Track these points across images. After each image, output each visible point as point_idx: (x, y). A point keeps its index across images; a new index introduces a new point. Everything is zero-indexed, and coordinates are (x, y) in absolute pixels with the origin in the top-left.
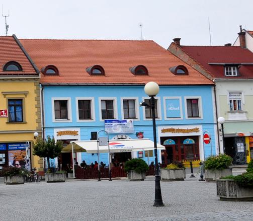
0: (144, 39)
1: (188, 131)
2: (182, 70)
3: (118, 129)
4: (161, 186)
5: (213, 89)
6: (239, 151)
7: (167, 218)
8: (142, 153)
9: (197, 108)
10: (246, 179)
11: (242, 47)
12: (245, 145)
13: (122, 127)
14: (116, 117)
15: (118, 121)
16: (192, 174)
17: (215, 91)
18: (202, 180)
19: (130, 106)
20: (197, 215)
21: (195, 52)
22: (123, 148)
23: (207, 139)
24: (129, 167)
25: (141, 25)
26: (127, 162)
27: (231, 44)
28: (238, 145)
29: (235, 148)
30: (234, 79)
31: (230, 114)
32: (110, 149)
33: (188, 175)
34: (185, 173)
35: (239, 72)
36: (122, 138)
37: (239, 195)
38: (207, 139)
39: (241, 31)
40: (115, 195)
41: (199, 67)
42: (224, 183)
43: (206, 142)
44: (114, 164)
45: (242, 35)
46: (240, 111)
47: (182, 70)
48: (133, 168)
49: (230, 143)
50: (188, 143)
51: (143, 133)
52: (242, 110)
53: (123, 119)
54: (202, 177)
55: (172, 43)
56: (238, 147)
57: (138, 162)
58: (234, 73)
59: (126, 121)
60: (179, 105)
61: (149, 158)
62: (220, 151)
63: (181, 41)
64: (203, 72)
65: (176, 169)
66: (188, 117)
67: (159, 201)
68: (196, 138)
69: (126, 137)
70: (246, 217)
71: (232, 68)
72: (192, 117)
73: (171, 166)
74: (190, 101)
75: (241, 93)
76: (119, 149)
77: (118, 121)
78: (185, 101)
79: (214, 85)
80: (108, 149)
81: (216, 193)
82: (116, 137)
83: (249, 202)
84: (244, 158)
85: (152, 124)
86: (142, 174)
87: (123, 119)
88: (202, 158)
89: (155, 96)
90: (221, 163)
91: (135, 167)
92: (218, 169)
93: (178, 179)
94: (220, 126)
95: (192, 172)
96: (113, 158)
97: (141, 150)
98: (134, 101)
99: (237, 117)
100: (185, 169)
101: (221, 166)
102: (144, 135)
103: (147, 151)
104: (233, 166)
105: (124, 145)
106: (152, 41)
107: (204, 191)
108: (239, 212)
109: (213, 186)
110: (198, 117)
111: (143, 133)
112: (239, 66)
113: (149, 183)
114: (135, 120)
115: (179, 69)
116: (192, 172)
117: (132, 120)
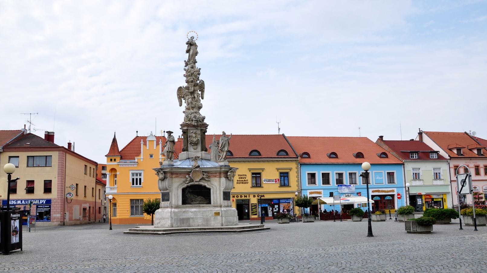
0: (362, 136)
1: (388, 191)
2: (384, 155)
3: (346, 190)
5: (403, 166)
8: (360, 205)
9: (393, 178)
10: (423, 220)
12: (422, 200)
13: (349, 189)
14: (345, 183)
15: (346, 186)
16: (390, 217)
17: (404, 167)
18: (396, 221)
19: (353, 177)
20: (393, 242)
21: (392, 144)
22: (349, 202)
24: (352, 213)
27: (414, 140)
29: (416, 202)
31: (413, 181)
33: (388, 218)
36: (348, 196)
37: (419, 230)
39: (420, 131)
40: (344, 230)
41: (394, 153)
43: (399, 198)
44: (344, 211)
45: (420, 134)
46: (419, 179)
47: (384, 155)
48: (355, 214)
49: (413, 198)
50: (388, 199)
51: (361, 192)
52: (420, 179)
53: (349, 184)
54: (396, 219)
56: (418, 201)
58: (416, 157)
63: (383, 138)
64: (397, 156)
66: (388, 183)
67: (370, 234)
68: (393, 196)
69: (351, 195)
70: (423, 243)
72: (390, 183)
73: (378, 213)
74: (389, 174)
75: (420, 169)
76: (346, 202)
77: (346, 186)
78: (386, 174)
79: (403, 164)
81: (405, 229)
84: (422, 208)
85: (366, 187)
86: (360, 217)
90: (408, 211)
91: (356, 213)
92: (406, 214)
93: (382, 221)
94: (407, 189)
95: (390, 216)
97: (360, 203)
98: (355, 173)
99: (417, 183)
100: (386, 214)
101: (408, 213)
102: (361, 194)
103: (363, 204)
105: (349, 200)
106: (366, 138)
110: (394, 183)
111: (361, 192)
112: (418, 153)
113: (365, 223)
116: (390, 216)
117: (354, 185)
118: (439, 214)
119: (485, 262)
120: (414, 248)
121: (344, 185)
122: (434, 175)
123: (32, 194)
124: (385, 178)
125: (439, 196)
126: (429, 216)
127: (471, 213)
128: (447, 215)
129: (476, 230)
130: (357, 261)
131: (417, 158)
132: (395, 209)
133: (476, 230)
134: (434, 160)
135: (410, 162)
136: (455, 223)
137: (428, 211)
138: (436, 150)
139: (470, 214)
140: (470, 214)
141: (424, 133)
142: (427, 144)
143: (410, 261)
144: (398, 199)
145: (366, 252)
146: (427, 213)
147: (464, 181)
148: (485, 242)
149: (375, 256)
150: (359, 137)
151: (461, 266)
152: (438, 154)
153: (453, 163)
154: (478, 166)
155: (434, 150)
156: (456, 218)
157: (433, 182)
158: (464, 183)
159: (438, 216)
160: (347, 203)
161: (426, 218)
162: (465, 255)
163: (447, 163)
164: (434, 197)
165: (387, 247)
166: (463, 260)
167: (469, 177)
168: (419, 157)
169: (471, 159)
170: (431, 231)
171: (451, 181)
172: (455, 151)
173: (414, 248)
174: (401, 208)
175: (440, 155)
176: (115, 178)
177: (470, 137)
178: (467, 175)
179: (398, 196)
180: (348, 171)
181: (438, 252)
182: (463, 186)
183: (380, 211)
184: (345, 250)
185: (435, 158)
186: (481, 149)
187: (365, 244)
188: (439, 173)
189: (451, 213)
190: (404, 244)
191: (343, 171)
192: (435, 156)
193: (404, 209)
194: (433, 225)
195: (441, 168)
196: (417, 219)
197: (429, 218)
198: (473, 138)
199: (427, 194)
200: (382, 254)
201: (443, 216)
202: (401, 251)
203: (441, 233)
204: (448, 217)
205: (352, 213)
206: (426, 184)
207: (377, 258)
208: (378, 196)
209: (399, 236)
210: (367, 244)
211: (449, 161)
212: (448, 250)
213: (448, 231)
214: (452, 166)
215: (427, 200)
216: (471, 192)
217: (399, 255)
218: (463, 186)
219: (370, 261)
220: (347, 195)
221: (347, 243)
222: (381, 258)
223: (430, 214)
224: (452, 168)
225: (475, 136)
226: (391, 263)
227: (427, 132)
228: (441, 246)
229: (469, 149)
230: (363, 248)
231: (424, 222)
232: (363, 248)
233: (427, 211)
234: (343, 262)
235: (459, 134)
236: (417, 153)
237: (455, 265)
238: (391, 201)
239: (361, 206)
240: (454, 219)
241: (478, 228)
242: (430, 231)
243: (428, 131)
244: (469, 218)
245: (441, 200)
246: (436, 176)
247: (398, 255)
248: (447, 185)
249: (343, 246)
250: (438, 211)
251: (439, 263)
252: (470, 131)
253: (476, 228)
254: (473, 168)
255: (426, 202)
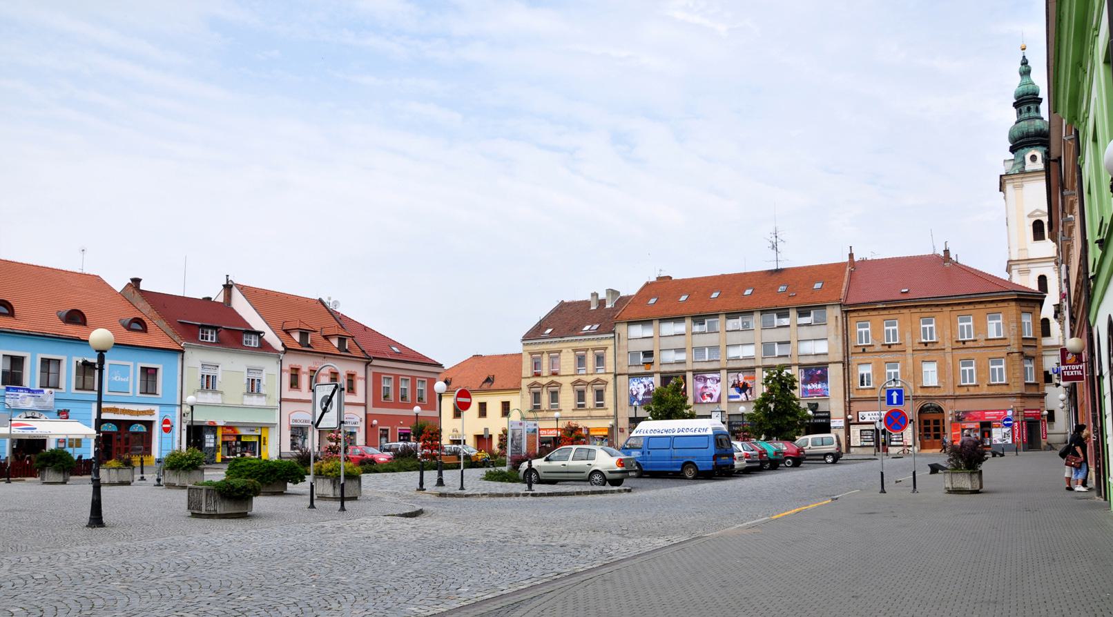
0: (87, 271)
1: (138, 413)
2: (138, 324)
3: (29, 402)
4: (102, 494)
5: (180, 356)
6: (207, 445)
7: (111, 548)
8: (64, 441)
9: (155, 381)
10: (233, 487)
11: (226, 305)
12: (216, 438)
13: (36, 401)
14: (27, 382)
15: (29, 390)
16: (141, 475)
17: (183, 359)
18: (159, 485)
19: (52, 368)
20: (159, 541)
21: (160, 302)
22: (35, 432)
23: (168, 426)
24: (43, 463)
25: (83, 250)
26: (40, 454)
27: (211, 299)
28: (207, 437)
29: (203, 441)
30: (211, 346)
31: (199, 393)
32: (12, 433)
33: (138, 476)
34: (133, 475)
35: (218, 338)
36: (33, 417)
37: (220, 510)
38: (168, 426)
39: (228, 282)
40: (18, 507)
41: (163, 324)
42: (199, 491)
43: (167, 430)
44: (16, 457)
45: (228, 287)
46: (214, 390)
47: (138, 324)
48: (50, 464)
49: (196, 433)
50: (136, 430)
51: (69, 411)
52: (217, 389)
53: (38, 388)
54: (159, 480)
55: (129, 283)
56: (207, 441)
57: (59, 456)
58: (212, 338)
59: (42, 391)
60: (129, 375)
61: (467, 471)
62: (181, 444)
63: (141, 283)
64: (169, 331)
65: (119, 468)
66: (141, 393)
67: (96, 518)
68: (149, 424)
69: (41, 416)
70: (234, 544)
71: (210, 331)
72: (147, 393)
73: (113, 463)
74: (145, 370)
75: (218, 366)
76: (26, 434)
77: (29, 390)
78: (139, 370)
79: (182, 352)
80: (9, 432)
81: (186, 507)
82: (23, 415)
83: (234, 520)
84: (213, 455)
85: (96, 399)
86: (64, 473)
87: (38, 388)
88: (156, 453)
89: (106, 351)
90: (190, 462)
91: (54, 463)
92: (184, 469)
93: (122, 483)
94: (186, 409)
95: (142, 473)
96: (15, 447)
97: (64, 437)
98: (59, 361)
99: (209, 398)
100: (134, 467)
101: (189, 466)
102: (70, 414)
103: (73, 439)
104: (207, 466)
105: (36, 429)
106: (98, 276)
107: (164, 502)
108: (222, 535)
109: (184, 494)
110: (155, 394)
111: (69, 411)
112: (219, 330)
113: (80, 489)
114: (57, 390)
115: (135, 322)
116: (142, 473)
117: (53, 390)
118: (262, 471)
119: (385, 589)
120: (216, 558)
121: (24, 389)
122: (248, 383)
123: (1049, 338)
124: (134, 381)
125: (254, 431)
126: (240, 476)
127: (331, 472)
128: (281, 476)
129: (343, 509)
130: (63, 605)
131: (214, 341)
132: (150, 454)
133: (343, 509)
134: (252, 351)
135: (198, 348)
136: (293, 492)
137: (239, 464)
138: (257, 328)
139: (329, 474)
140: (329, 474)
141: (237, 288)
142: (240, 314)
143: (214, 594)
144: (164, 433)
145: (86, 572)
146: (236, 468)
147: (329, 401)
148: (370, 537)
149: (116, 584)
150: (80, 274)
151: (339, 603)
152: (260, 338)
153: (290, 361)
154: (297, 370)
155: (252, 328)
156: (297, 483)
157: (243, 398)
158: (327, 405)
159: (260, 477)
160: (29, 435)
161: (239, 482)
162: (338, 573)
163: (277, 360)
164: (242, 432)
165: (145, 556)
166: (341, 587)
167: (341, 391)
168: (261, 344)
169: (325, 358)
170: (249, 513)
171: (281, 400)
172: (296, 336)
173: (216, 558)
174: (173, 455)
175: (264, 339)
176: (868, 375)
177: (328, 310)
178: (336, 387)
179: (165, 426)
180: (41, 353)
181: (278, 567)
182: (325, 411)
183: (120, 459)
184: (21, 568)
185: (253, 345)
186: (345, 339)
187: (81, 547)
188: (259, 380)
189: (288, 471)
190: (188, 546)
191: (62, 355)
192: (254, 342)
193: (181, 456)
194: (254, 498)
195: (220, 366)
196: (218, 483)
197: (246, 482)
198: (333, 314)
199: (229, 425)
200: (134, 577)
201: (272, 476)
202: (185, 566)
203: (269, 517)
204: (282, 480)
205: (43, 463)
206: (228, 402)
207: (121, 591)
208: (113, 423)
209: (172, 526)
210: (88, 547)
211: (282, 355)
212: (297, 559)
213: (284, 512)
214: (286, 367)
215: (227, 439)
216: (340, 424)
217: (182, 579)
218: (325, 411)
219: (101, 602)
220: (29, 414)
221: (29, 548)
222: (134, 589)
223: (243, 471)
224: (305, 375)
225: (337, 310)
226: (163, 603)
227: (244, 286)
228: (280, 550)
229: (323, 336)
230: (78, 562)
231: (234, 490)
232: (78, 562)
233: (236, 465)
234: (17, 609)
235: (307, 300)
236: (216, 330)
237: (326, 601)
238: (142, 437)
239: (67, 444)
240: (294, 483)
241: (347, 504)
242: (247, 513)
243: (244, 284)
244: (328, 482)
245: (255, 439)
246: (252, 386)
247: (179, 578)
248: (273, 409)
249: (14, 559)
250: (262, 464)
251: (287, 599)
252: (329, 299)
253: (342, 505)
254: (327, 375)
255: (224, 443)
